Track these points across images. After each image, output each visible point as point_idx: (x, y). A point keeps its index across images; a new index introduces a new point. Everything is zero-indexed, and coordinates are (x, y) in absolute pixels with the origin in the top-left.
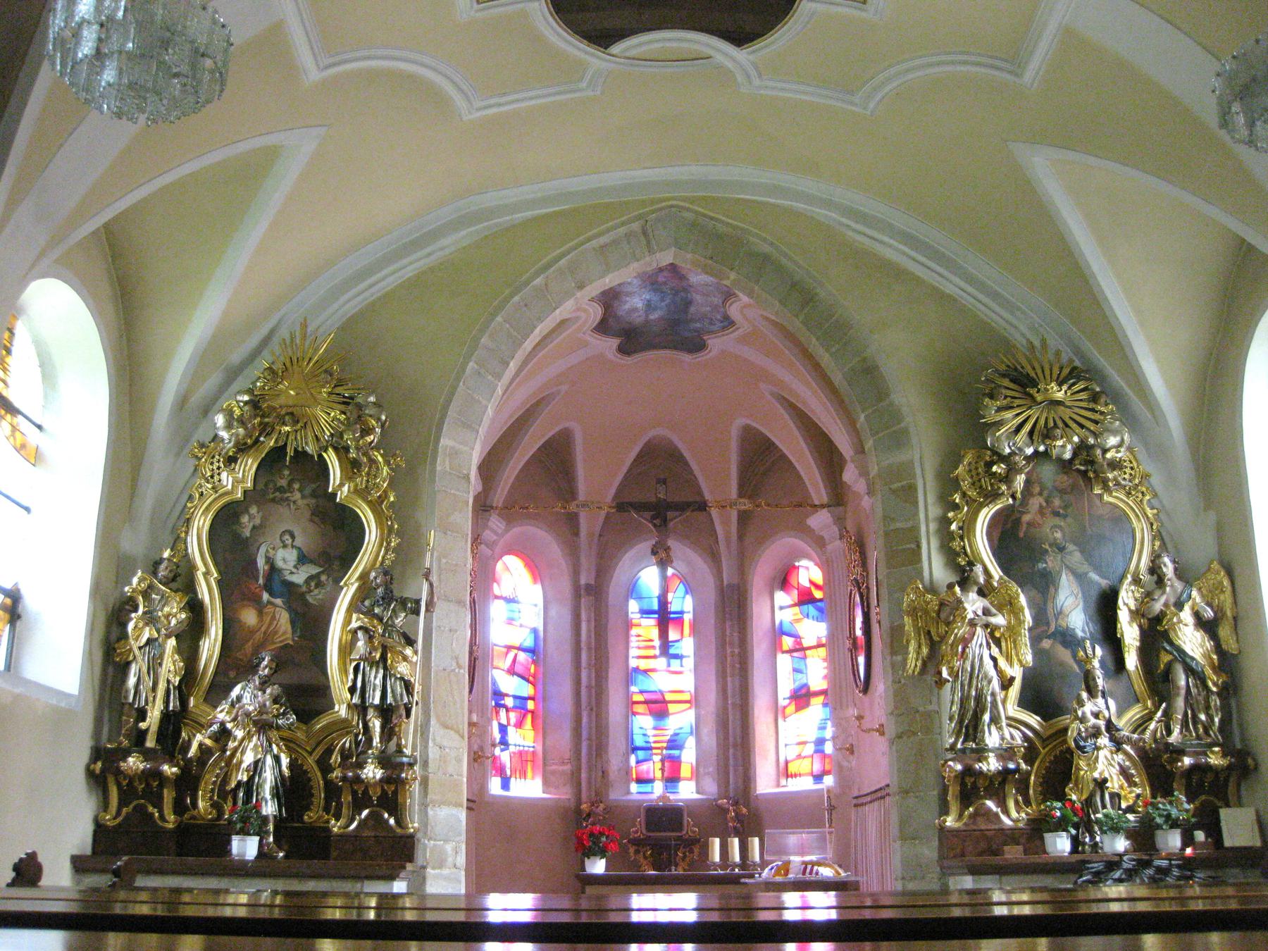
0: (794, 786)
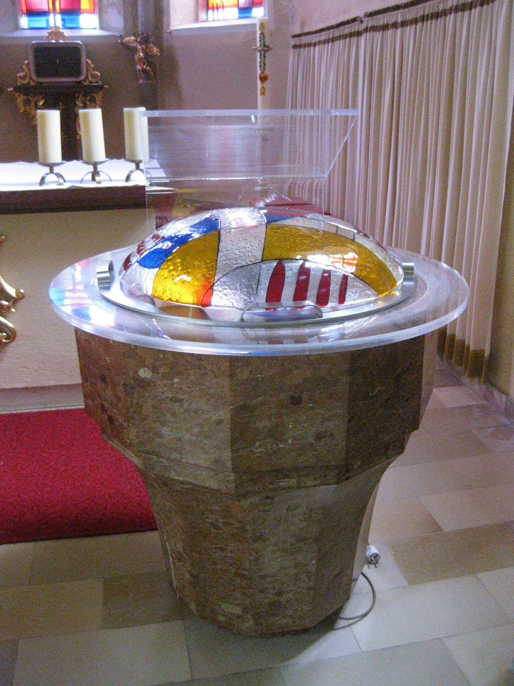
0: (215, 20)
